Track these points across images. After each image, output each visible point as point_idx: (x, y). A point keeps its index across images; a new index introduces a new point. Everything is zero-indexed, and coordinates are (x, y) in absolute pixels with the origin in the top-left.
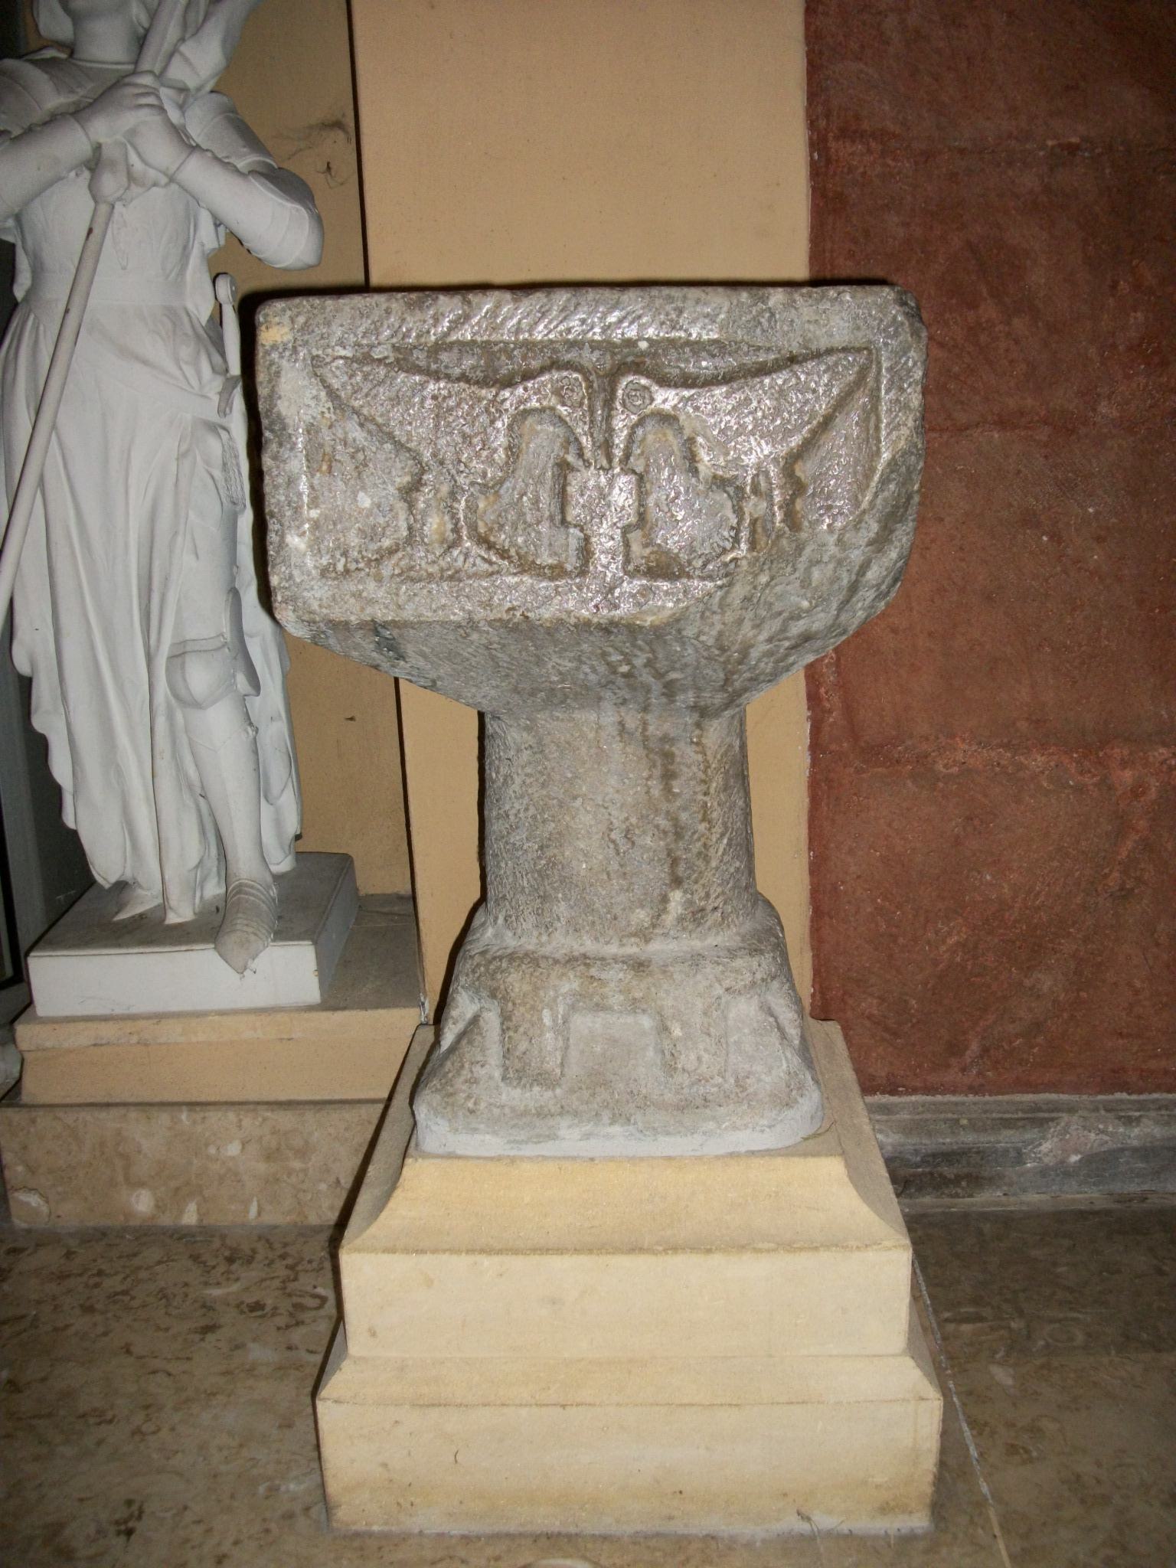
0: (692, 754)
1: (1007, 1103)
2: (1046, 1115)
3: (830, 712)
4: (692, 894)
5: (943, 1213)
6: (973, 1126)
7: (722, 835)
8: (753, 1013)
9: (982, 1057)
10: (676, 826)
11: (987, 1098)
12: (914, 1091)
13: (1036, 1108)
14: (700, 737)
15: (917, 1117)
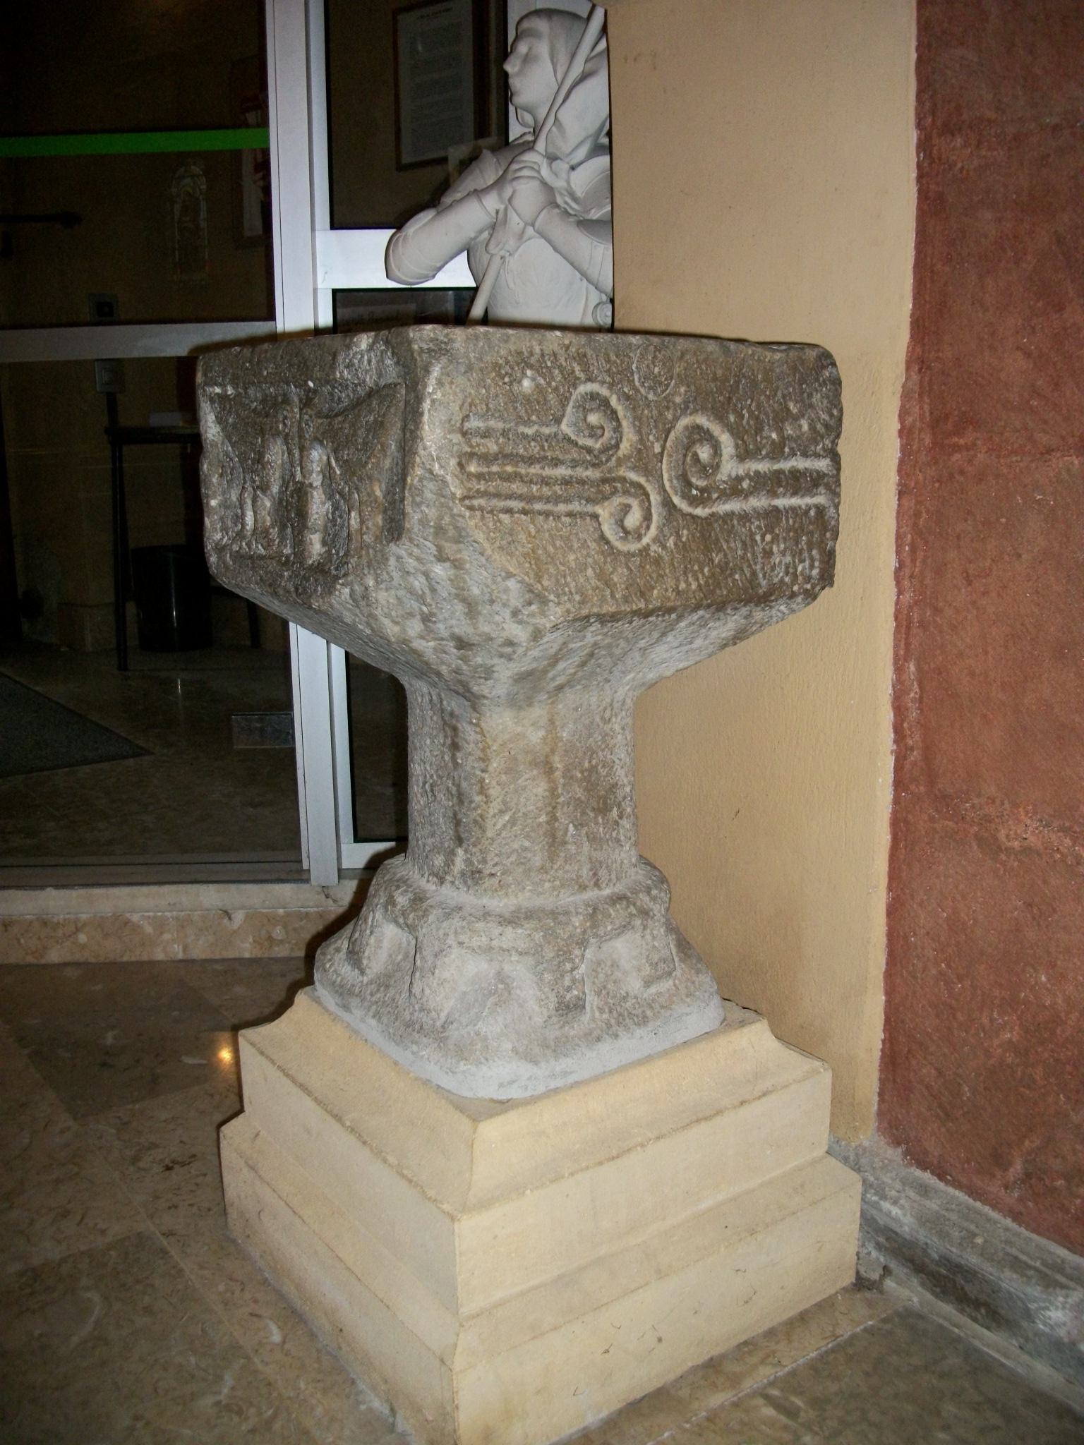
0: (473, 733)
1: (1037, 1246)
2: (1063, 1280)
3: (912, 749)
4: (471, 855)
5: (941, 1326)
6: (983, 1252)
7: (502, 812)
8: (491, 975)
9: (1023, 1182)
10: (458, 790)
11: (1022, 1230)
12: (957, 1185)
13: (1059, 1268)
14: (479, 719)
15: (943, 1212)
